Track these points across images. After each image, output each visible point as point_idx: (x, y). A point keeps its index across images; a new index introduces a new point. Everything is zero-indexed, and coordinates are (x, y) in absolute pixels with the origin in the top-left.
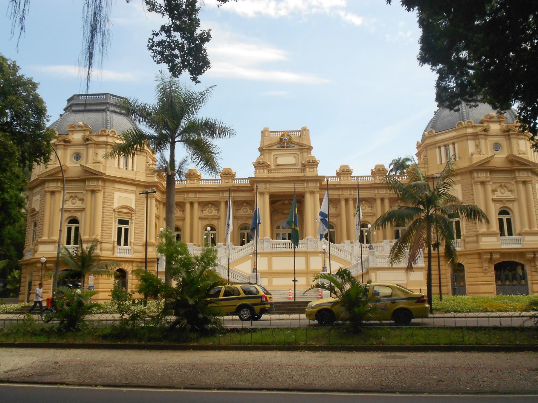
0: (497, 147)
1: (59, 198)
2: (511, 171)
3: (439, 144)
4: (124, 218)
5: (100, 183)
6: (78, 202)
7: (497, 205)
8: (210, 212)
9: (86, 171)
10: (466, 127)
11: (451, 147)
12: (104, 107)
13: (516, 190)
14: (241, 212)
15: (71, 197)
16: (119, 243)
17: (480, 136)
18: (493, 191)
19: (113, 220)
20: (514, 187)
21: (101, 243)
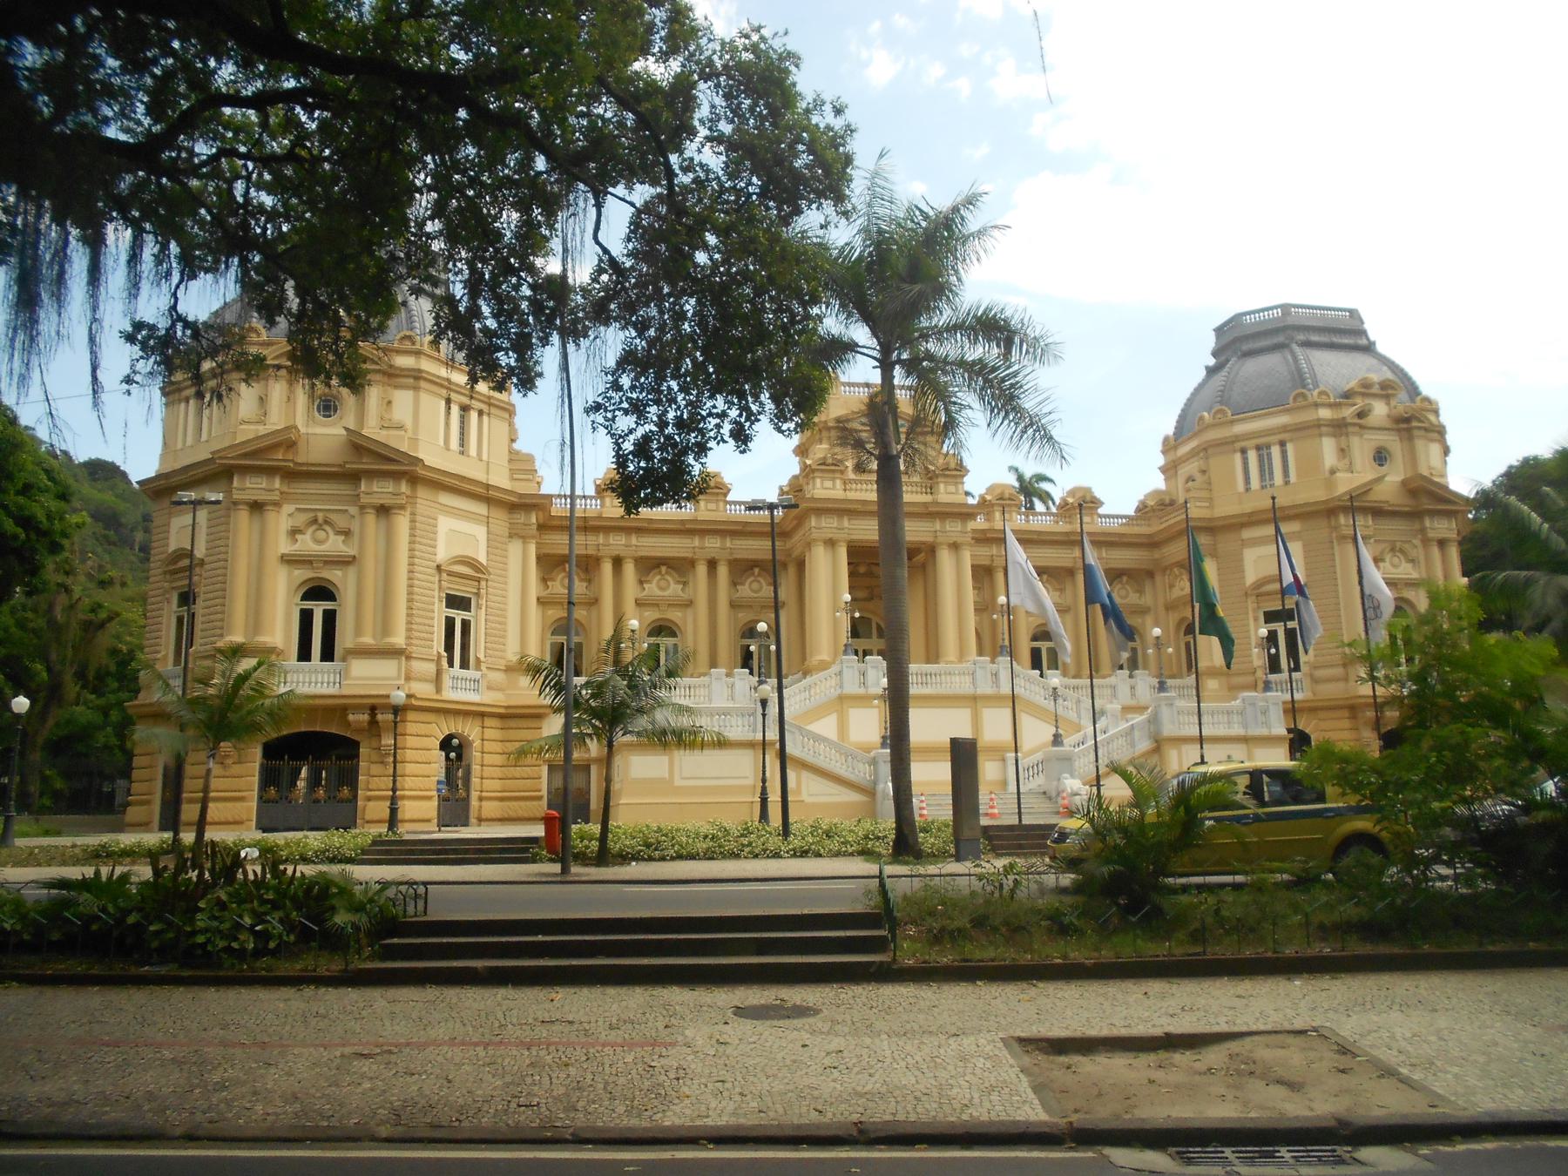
0: (1381, 457)
1: (281, 521)
2: (1415, 515)
3: (1243, 444)
4: (462, 589)
5: (404, 487)
6: (332, 537)
7: (297, 572)
8: (664, 587)
9: (359, 446)
10: (1316, 405)
11: (1276, 451)
12: (1280, 339)
13: (1422, 559)
14: (745, 591)
15: (315, 521)
16: (451, 664)
17: (1351, 429)
18: (294, 532)
19: (436, 594)
20: (1419, 553)
21: (408, 658)
